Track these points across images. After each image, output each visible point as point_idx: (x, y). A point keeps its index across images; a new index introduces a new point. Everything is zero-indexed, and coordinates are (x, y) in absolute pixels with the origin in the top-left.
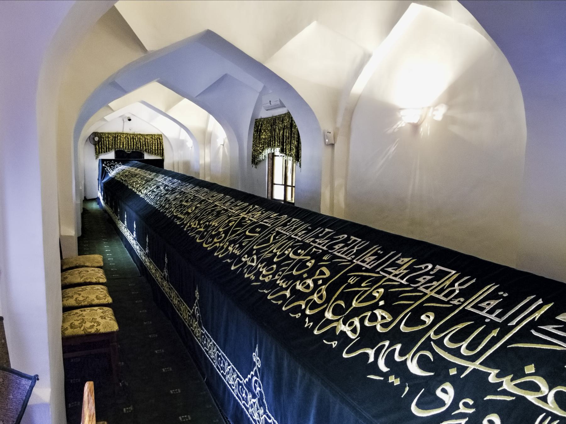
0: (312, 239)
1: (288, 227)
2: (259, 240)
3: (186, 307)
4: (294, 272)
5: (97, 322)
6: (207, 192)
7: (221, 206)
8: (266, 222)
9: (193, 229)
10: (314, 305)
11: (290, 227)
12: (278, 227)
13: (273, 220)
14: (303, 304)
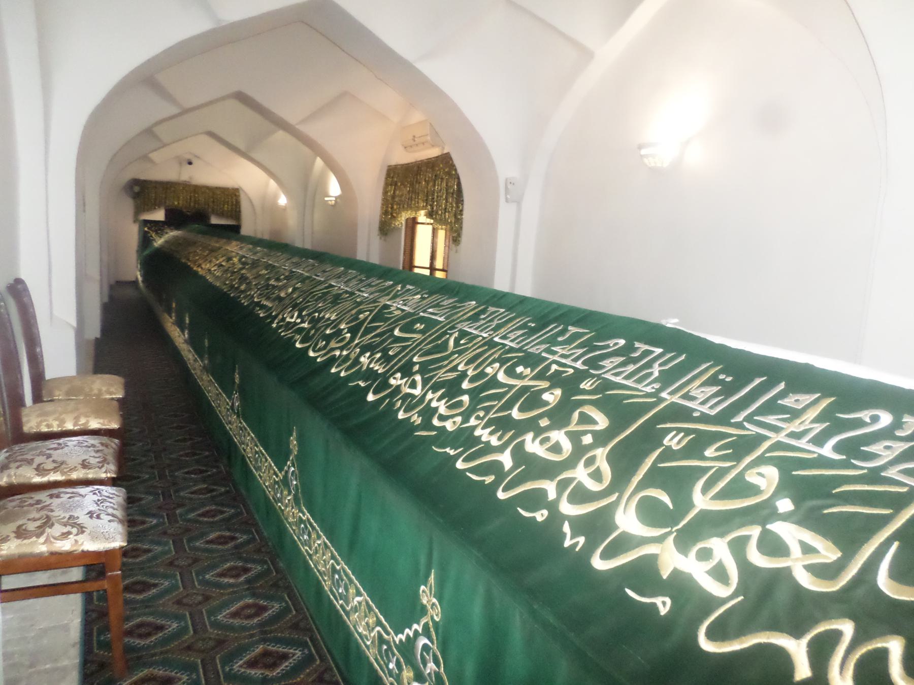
0: (544, 347)
1: (483, 322)
2: (425, 345)
3: (271, 465)
4: (515, 414)
5: (78, 525)
6: (313, 266)
7: (339, 287)
8: (431, 313)
9: (289, 326)
10: (580, 495)
11: (486, 323)
12: (461, 322)
13: (447, 310)
14: (550, 488)
